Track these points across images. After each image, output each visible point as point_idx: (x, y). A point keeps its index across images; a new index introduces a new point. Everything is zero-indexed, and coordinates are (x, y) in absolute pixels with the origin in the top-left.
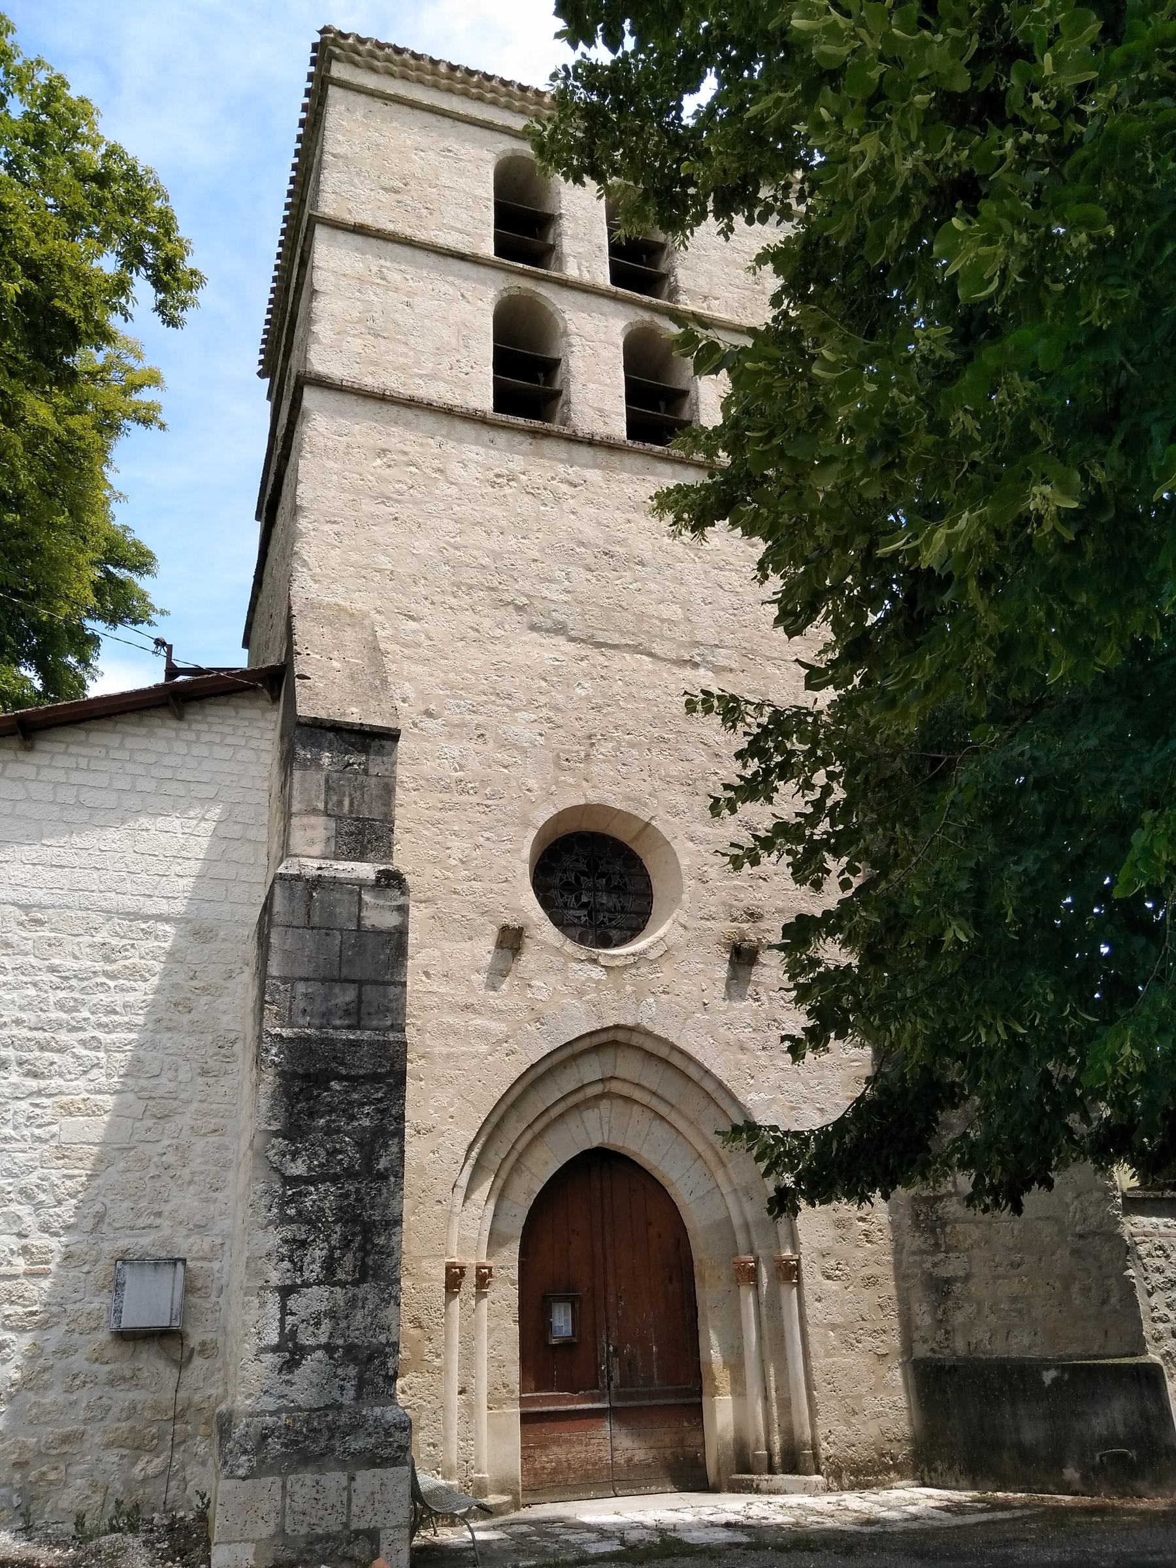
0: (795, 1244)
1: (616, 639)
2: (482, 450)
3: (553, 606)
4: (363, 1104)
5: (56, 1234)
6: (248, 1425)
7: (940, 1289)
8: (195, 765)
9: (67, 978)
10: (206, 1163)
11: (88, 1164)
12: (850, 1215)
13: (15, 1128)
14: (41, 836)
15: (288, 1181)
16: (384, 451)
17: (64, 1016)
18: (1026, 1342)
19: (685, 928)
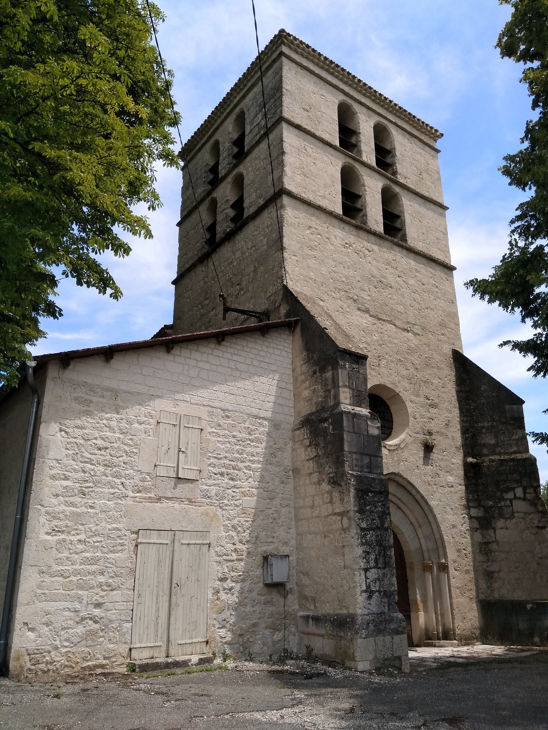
0: (446, 557)
1: (384, 318)
2: (341, 232)
3: (365, 301)
4: (378, 502)
5: (244, 544)
6: (362, 619)
7: (489, 575)
8: (269, 356)
9: (238, 441)
10: (286, 518)
11: (252, 516)
12: (461, 548)
13: (228, 501)
14: (226, 381)
15: (362, 529)
16: (310, 227)
17: (239, 456)
18: (520, 594)
19: (411, 436)
